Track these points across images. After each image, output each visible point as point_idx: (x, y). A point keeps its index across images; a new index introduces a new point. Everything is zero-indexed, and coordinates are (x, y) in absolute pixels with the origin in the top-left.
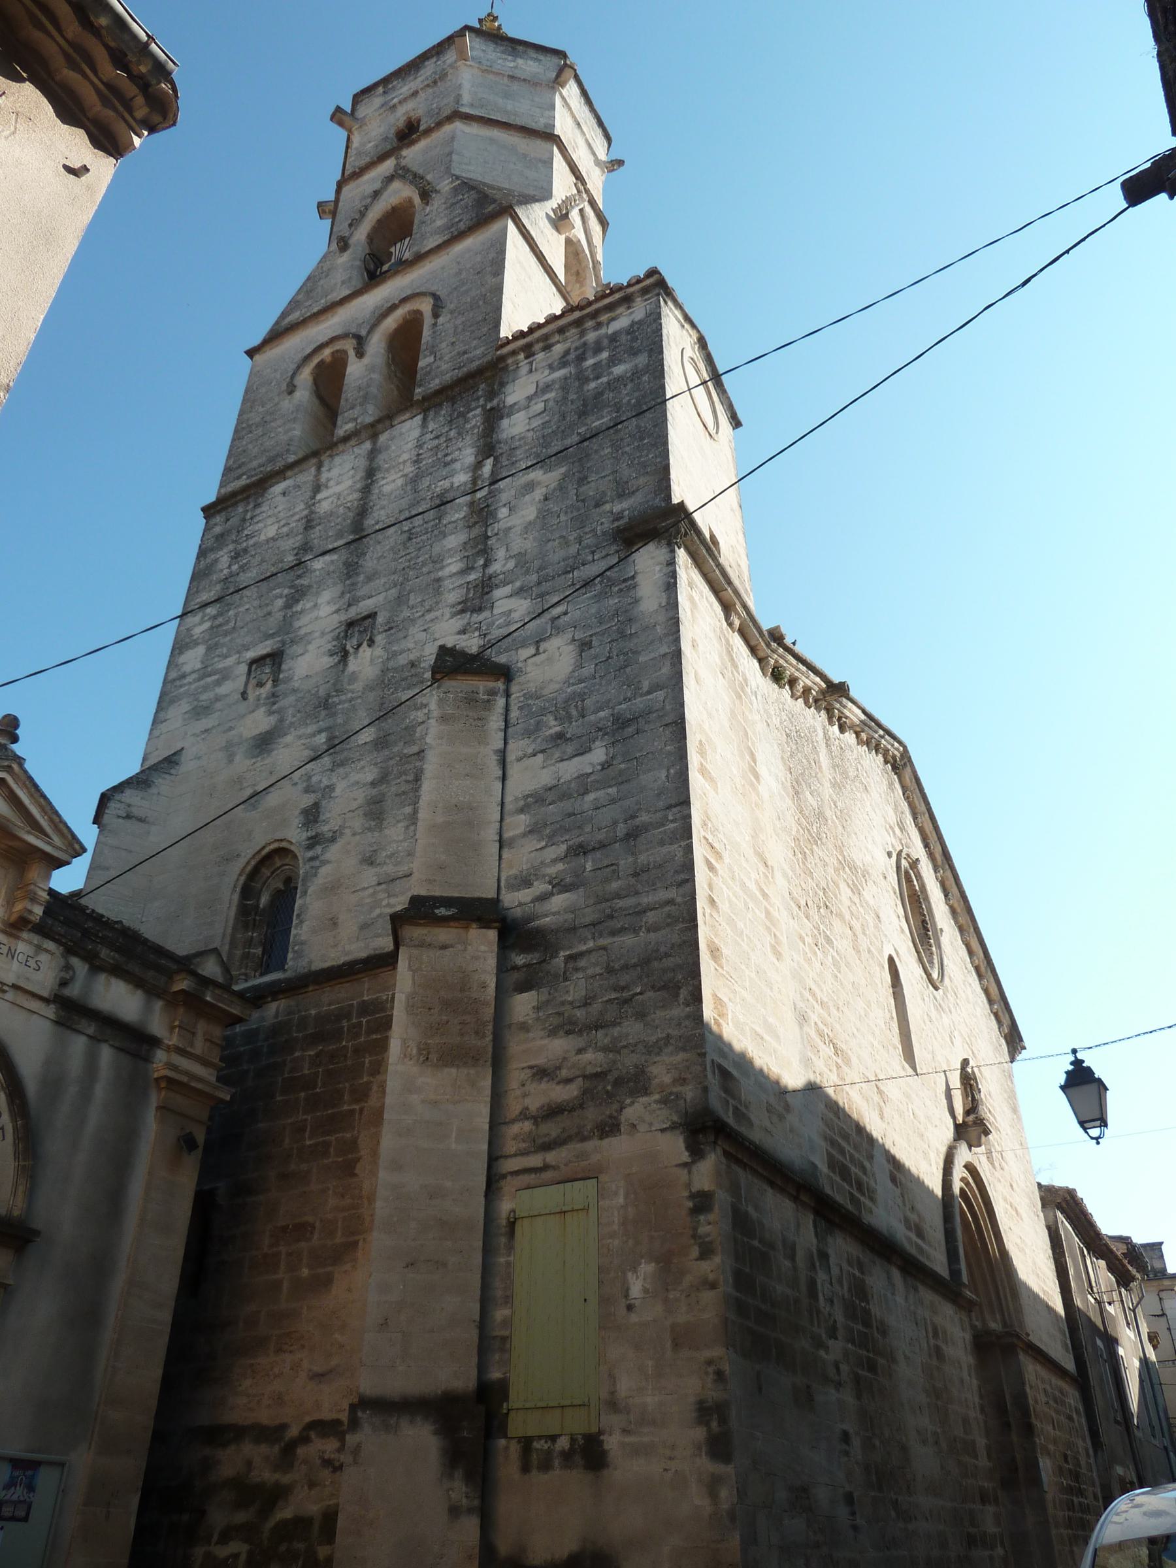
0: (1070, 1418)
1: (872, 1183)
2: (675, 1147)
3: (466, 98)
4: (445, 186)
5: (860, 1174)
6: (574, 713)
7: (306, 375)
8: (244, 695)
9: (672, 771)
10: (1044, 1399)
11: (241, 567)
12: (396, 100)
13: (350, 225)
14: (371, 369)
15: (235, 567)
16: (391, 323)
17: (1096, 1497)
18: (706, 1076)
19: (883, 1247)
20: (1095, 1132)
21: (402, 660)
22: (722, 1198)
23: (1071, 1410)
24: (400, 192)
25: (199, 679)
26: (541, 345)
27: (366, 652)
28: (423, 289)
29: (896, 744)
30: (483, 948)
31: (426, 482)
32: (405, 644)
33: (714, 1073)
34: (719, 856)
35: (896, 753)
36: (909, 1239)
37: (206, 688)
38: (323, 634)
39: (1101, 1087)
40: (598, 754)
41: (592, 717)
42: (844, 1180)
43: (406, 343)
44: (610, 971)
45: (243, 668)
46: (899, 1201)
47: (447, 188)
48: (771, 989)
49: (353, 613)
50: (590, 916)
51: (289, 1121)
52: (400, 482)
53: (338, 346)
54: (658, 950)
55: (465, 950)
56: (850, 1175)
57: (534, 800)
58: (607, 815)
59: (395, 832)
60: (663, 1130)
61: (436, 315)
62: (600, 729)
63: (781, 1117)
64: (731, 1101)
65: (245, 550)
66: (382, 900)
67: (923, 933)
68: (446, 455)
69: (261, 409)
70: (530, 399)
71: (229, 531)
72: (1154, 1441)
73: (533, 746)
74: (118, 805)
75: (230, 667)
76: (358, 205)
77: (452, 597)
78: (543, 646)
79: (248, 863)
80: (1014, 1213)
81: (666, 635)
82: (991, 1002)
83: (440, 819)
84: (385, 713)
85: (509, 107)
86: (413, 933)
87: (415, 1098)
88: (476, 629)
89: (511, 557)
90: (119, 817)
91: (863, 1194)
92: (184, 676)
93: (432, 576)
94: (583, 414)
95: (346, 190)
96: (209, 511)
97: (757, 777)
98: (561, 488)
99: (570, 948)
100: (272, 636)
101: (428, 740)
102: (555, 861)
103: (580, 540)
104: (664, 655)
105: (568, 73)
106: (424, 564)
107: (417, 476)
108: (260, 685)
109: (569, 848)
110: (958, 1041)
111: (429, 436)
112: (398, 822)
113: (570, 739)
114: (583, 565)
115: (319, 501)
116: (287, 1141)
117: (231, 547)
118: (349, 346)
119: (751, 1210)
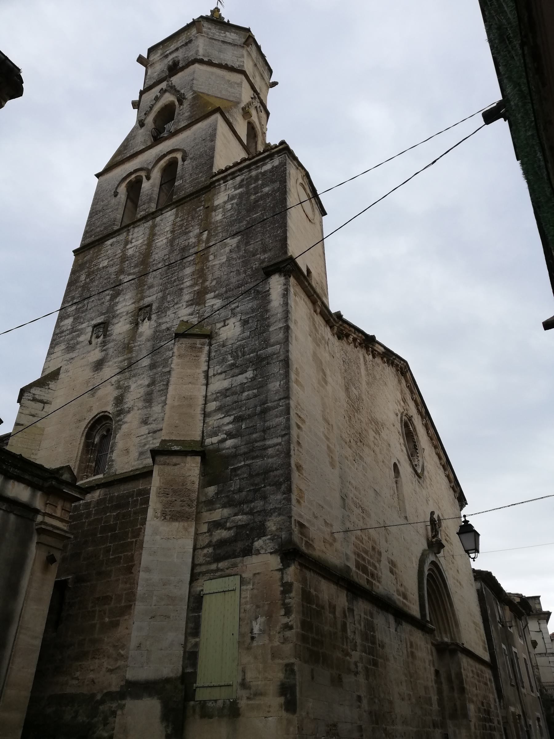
0: (486, 684)
1: (380, 574)
2: (275, 561)
3: (201, 52)
4: (189, 96)
5: (373, 570)
6: (240, 354)
7: (123, 186)
8: (90, 343)
9: (282, 382)
10: (471, 675)
11: (91, 280)
12: (168, 52)
13: (145, 114)
14: (153, 186)
15: (88, 280)
16: (163, 163)
17: (499, 723)
18: (291, 527)
19: (384, 604)
20: (472, 555)
21: (164, 327)
22: (297, 586)
23: (486, 680)
24: (169, 98)
25: (71, 333)
26: (231, 177)
27: (146, 323)
28: (178, 147)
29: (402, 362)
30: (193, 465)
31: (177, 241)
32: (164, 320)
33: (296, 525)
34: (303, 421)
35: (402, 366)
36: (399, 599)
37: (72, 339)
38: (127, 313)
39: (477, 535)
40: (250, 374)
41: (248, 356)
42: (364, 572)
43: (170, 171)
44: (251, 476)
45: (90, 329)
46: (395, 582)
47: (190, 97)
48: (329, 483)
49: (141, 304)
50: (243, 449)
51: (103, 546)
52: (165, 241)
53: (138, 174)
54: (272, 467)
55: (185, 466)
56: (368, 570)
57: (225, 393)
58: (252, 402)
59: (157, 408)
60: (271, 553)
61: (184, 160)
62: (251, 362)
63: (331, 545)
64: (304, 539)
65: (93, 272)
66: (150, 441)
67: (413, 450)
68: (187, 229)
69: (102, 203)
70: (225, 203)
71: (86, 263)
72: (532, 694)
73: (221, 369)
74: (29, 394)
75: (85, 328)
76: (149, 104)
77: (186, 297)
78: (227, 322)
79: (89, 422)
80: (459, 584)
81: (282, 319)
82: (450, 482)
83: (176, 404)
84: (155, 351)
85: (222, 57)
86: (160, 459)
87: (158, 538)
88: (198, 313)
89: (215, 279)
90: (29, 400)
91: (375, 579)
92: (63, 332)
93: (178, 287)
94: (249, 211)
95: (144, 96)
96: (77, 252)
97: (326, 383)
98: (238, 246)
99: (233, 465)
100: (104, 314)
101: (172, 366)
102: (228, 424)
103: (245, 272)
104: (280, 328)
105: (251, 40)
106: (175, 281)
107: (173, 238)
108: (98, 337)
109: (235, 417)
110: (431, 502)
111: (178, 219)
112: (159, 404)
113: (237, 367)
114: (247, 284)
115: (128, 250)
116: (102, 556)
117: (86, 270)
118: (143, 174)
119: (312, 591)
